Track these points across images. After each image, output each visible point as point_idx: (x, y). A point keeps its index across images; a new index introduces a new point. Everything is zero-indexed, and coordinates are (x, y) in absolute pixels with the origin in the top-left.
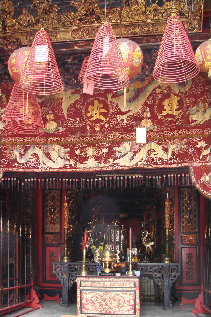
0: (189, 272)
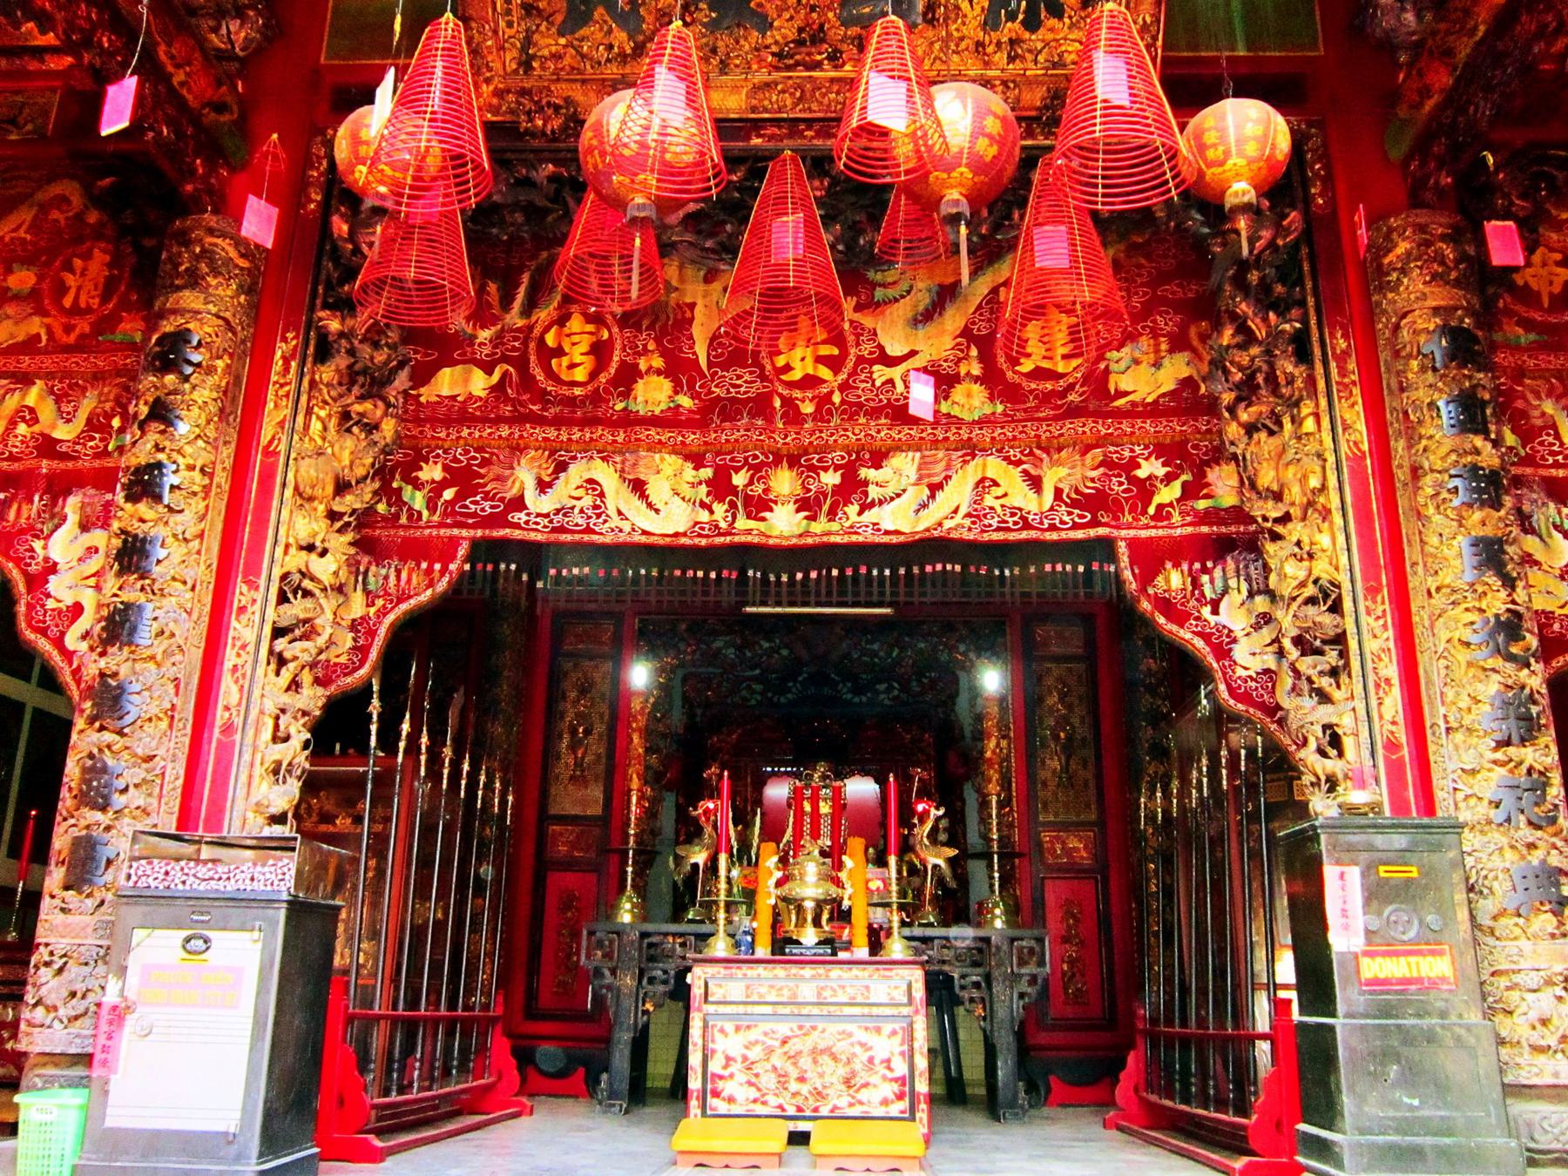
0: (1073, 975)
